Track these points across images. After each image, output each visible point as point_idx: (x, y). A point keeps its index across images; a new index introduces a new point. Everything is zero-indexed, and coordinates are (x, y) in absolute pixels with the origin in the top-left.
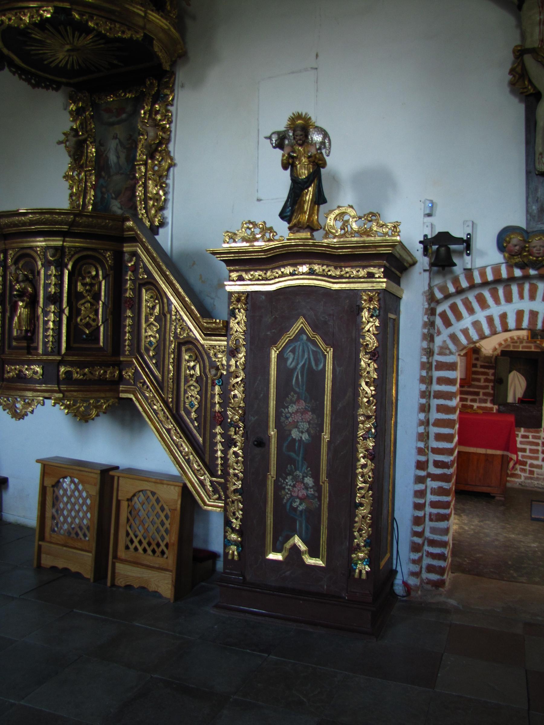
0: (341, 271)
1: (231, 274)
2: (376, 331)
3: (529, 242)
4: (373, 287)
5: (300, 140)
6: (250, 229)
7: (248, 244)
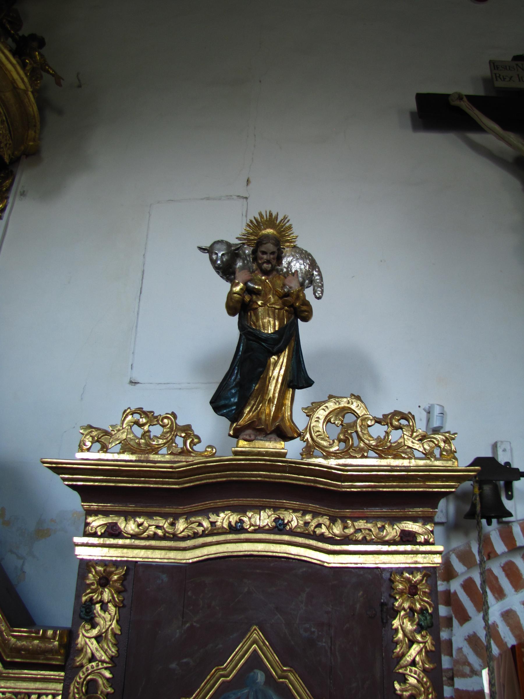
0: (345, 527)
1: (90, 519)
2: (430, 662)
4: (416, 563)
5: (268, 262)
6: (141, 426)
7: (133, 457)
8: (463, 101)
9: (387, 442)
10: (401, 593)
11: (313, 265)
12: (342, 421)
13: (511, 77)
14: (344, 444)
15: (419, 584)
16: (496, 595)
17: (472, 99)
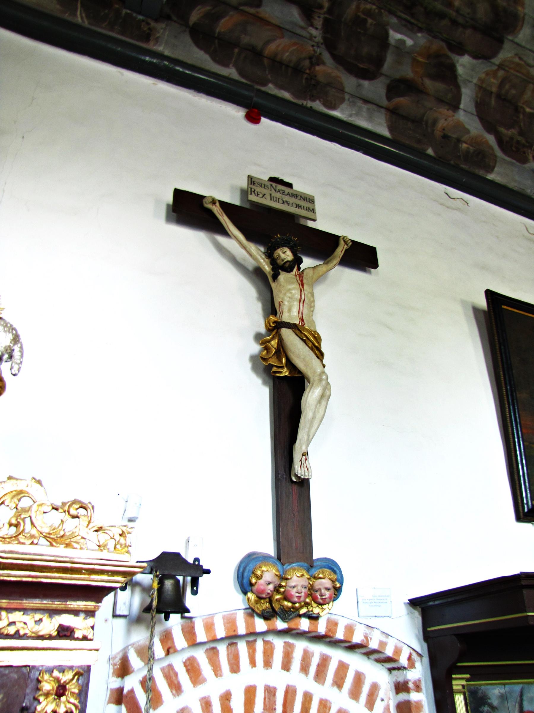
3: (287, 579)
8: (216, 206)
9: (60, 530)
10: (47, 695)
11: (16, 339)
12: (17, 505)
13: (265, 195)
14: (15, 528)
15: (68, 683)
16: (174, 692)
17: (225, 206)
